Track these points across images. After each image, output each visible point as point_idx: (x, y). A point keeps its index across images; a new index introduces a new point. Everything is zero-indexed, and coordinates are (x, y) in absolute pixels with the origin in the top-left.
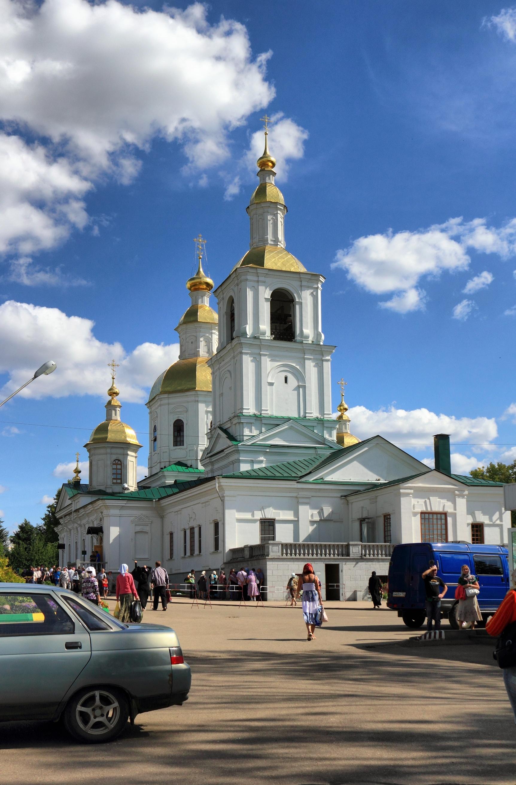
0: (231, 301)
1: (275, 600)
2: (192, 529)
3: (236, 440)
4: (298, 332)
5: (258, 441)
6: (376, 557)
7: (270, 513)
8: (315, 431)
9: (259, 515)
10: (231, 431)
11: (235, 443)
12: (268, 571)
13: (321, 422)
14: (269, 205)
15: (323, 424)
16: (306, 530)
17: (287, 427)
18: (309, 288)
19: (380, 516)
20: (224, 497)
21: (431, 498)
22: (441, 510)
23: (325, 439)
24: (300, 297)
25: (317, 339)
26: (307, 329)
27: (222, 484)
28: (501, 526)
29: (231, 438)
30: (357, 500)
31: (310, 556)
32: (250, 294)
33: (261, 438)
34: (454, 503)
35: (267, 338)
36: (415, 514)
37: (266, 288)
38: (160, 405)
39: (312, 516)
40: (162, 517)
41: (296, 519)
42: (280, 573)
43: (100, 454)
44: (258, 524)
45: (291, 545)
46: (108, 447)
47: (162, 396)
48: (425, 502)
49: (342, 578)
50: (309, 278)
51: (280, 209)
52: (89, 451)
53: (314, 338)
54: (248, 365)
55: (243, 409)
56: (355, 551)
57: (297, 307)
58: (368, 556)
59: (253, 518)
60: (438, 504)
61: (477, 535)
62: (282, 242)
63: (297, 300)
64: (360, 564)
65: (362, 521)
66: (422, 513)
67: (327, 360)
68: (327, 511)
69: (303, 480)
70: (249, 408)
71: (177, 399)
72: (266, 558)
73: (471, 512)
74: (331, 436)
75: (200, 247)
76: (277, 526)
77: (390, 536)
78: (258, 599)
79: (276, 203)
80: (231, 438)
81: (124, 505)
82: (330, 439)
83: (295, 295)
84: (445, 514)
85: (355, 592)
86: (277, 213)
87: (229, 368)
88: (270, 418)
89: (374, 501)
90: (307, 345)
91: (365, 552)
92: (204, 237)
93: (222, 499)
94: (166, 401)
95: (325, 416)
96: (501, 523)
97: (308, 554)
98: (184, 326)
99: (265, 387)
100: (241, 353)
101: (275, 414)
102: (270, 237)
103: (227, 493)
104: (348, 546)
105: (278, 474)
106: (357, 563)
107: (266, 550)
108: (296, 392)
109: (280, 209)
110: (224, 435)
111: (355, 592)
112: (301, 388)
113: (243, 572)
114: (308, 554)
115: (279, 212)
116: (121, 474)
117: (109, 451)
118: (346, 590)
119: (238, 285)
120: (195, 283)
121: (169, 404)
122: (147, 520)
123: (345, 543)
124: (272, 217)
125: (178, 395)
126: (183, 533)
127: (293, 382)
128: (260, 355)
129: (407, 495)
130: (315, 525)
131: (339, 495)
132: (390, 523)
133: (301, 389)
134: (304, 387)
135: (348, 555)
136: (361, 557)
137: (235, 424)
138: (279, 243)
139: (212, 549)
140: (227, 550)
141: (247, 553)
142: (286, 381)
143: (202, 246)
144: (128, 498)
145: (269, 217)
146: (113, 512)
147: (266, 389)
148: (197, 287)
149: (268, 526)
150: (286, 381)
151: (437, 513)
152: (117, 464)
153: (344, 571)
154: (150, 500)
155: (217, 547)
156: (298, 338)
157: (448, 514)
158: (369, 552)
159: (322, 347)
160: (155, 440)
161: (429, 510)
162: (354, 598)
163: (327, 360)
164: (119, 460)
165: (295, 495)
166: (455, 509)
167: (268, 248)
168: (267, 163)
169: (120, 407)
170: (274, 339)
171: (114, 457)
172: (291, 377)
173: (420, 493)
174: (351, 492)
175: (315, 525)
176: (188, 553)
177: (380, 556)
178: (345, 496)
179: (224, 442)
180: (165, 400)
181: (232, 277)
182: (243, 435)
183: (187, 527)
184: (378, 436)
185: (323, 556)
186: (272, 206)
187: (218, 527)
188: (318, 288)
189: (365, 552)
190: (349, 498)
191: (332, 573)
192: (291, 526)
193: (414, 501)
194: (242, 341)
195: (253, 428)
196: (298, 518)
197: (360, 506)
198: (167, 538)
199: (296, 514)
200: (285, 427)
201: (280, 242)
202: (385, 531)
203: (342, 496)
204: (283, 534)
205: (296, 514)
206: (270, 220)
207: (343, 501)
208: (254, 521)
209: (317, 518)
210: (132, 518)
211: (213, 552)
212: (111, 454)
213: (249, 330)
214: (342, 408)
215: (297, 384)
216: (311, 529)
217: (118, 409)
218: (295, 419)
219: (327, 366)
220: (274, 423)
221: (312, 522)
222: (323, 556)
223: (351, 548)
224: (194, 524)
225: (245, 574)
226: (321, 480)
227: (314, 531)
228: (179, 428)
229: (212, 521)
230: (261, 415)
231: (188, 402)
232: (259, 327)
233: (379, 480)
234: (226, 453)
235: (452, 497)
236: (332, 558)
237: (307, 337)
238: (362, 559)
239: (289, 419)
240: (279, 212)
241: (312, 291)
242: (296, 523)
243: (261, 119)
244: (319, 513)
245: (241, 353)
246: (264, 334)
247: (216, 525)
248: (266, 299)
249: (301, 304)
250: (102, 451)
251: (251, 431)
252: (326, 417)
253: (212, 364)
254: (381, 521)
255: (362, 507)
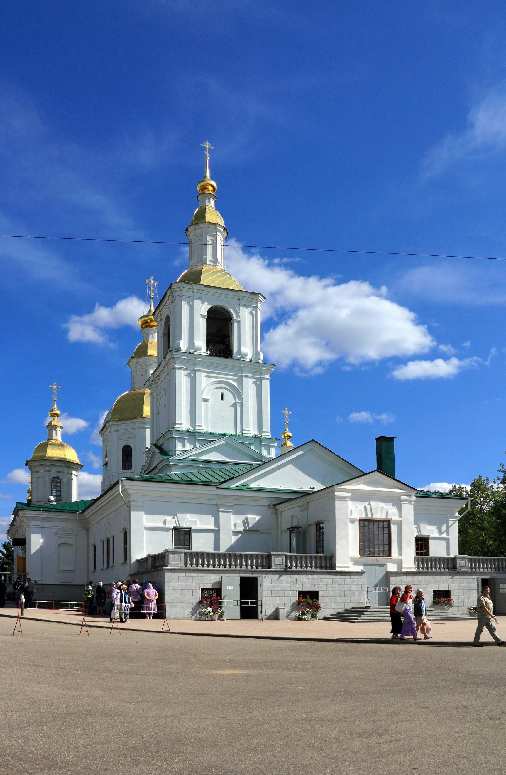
0: (168, 319)
1: (175, 619)
2: (108, 540)
3: (168, 455)
4: (235, 349)
5: (193, 454)
6: (304, 569)
7: (187, 520)
8: (253, 447)
9: (171, 522)
10: (164, 447)
11: (166, 457)
12: (166, 584)
13: (259, 440)
14: (208, 226)
15: (261, 442)
16: (228, 541)
17: (223, 442)
18: (247, 306)
19: (311, 525)
20: (129, 502)
21: (372, 503)
22: (383, 517)
23: (262, 456)
24: (238, 314)
25: (256, 357)
26: (245, 346)
27: (126, 487)
28: (447, 540)
29: (163, 452)
30: (287, 508)
31: (222, 568)
32: (185, 308)
33: (194, 453)
34: (400, 509)
35: (202, 354)
36: (353, 521)
37: (203, 303)
38: (110, 432)
39: (235, 525)
40: (88, 530)
41: (217, 529)
42: (182, 589)
43: (40, 472)
44: (171, 533)
45: (208, 554)
46: (46, 464)
47: (111, 423)
48: (365, 508)
49: (261, 593)
50: (248, 296)
51: (220, 231)
52: (30, 469)
53: (253, 356)
54: (182, 379)
55: (176, 424)
56: (278, 562)
57: (235, 325)
58: (294, 569)
59: (165, 527)
60: (381, 511)
61: (421, 549)
62: (222, 265)
63: (235, 318)
64: (285, 577)
65: (291, 530)
66: (360, 520)
67: (266, 379)
68: (254, 519)
69: (224, 485)
70: (183, 422)
71: (126, 426)
72: (163, 569)
73: (416, 522)
74: (269, 453)
75: (152, 288)
76: (193, 535)
77: (323, 546)
78: (155, 617)
79: (215, 224)
80: (163, 452)
81: (45, 516)
82: (268, 456)
83: (232, 310)
84: (389, 522)
85: (277, 610)
86: (217, 234)
87: (163, 387)
88: (205, 434)
89: (305, 508)
90: (246, 363)
91: (291, 563)
92: (155, 279)
93: (128, 504)
94: (115, 428)
95: (263, 434)
96: (448, 537)
97: (219, 565)
98: (134, 360)
99: (198, 401)
100: (175, 368)
101: (210, 430)
102: (209, 257)
103: (132, 498)
104: (269, 557)
105: (195, 479)
106: (280, 576)
107: (166, 558)
108: (233, 409)
109: (220, 231)
110: (157, 451)
111: (277, 610)
112: (239, 405)
113: (137, 585)
114: (219, 565)
115: (218, 233)
116: (61, 491)
117: (47, 468)
118: (266, 608)
119: (173, 301)
120: (146, 320)
121: (118, 431)
122: (72, 532)
123: (265, 553)
124: (211, 238)
125: (126, 422)
126: (102, 543)
127: (229, 398)
128: (195, 371)
129: (344, 498)
130: (240, 535)
131: (267, 504)
132: (323, 532)
133: (238, 407)
134: (242, 405)
135: (270, 567)
136: (286, 569)
137: (168, 439)
138: (217, 264)
139: (122, 561)
140: (133, 560)
141: (149, 562)
142: (222, 398)
143: (154, 286)
144: (49, 510)
145: (208, 238)
146: (33, 523)
147: (201, 406)
148: (148, 324)
149: (183, 536)
150: (222, 398)
151: (379, 521)
152: (56, 482)
153: (263, 586)
154: (74, 512)
155: (126, 560)
156: (235, 356)
157: (391, 522)
158: (296, 563)
159: (261, 365)
160: (106, 464)
161: (370, 517)
162: (275, 616)
163: (266, 379)
164: (58, 478)
165: (215, 502)
166: (400, 516)
167: (205, 268)
168: (207, 187)
169: (62, 427)
170: (210, 355)
171: (53, 475)
172: (228, 396)
173: (358, 496)
174: (280, 500)
175: (240, 535)
176: (106, 566)
177: (309, 569)
178: (275, 505)
179: (159, 457)
180: (114, 426)
181: (168, 294)
182: (175, 450)
183: (104, 538)
184: (313, 440)
185: (238, 568)
186: (211, 226)
187: (126, 535)
188: (257, 307)
189: (291, 563)
190: (278, 507)
191: (249, 589)
192: (212, 535)
193: (351, 505)
194: (175, 356)
195: (186, 441)
196: (219, 528)
197: (290, 515)
198: (92, 549)
199: (217, 523)
200: (222, 442)
201: (219, 263)
202: (317, 541)
203: (270, 505)
204: (201, 544)
205: (217, 523)
206: (209, 241)
207: (271, 510)
208: (168, 529)
209: (242, 529)
210: (55, 530)
211: (123, 563)
212: (50, 471)
213: (184, 345)
214: (286, 435)
215: (234, 401)
216: (234, 539)
217: (59, 429)
218: (231, 436)
219: (266, 385)
220: (208, 438)
221: (236, 533)
222: (238, 568)
223: (273, 558)
224: (109, 535)
225: (138, 586)
226: (246, 487)
227: (237, 542)
228: (127, 452)
229: (121, 530)
230: (195, 430)
231: (136, 429)
232: (194, 343)
233: (313, 488)
234: (159, 468)
235: (397, 502)
236: (250, 570)
237: (246, 355)
238: (286, 571)
239: (225, 435)
240: (218, 233)
241: (251, 309)
242: (216, 533)
243: (202, 145)
244: (243, 522)
245: (175, 368)
246: (200, 349)
247: (125, 533)
248: (202, 316)
249: (239, 322)
250: (41, 468)
251: (184, 446)
252: (264, 435)
253: (150, 385)
254: (313, 530)
255: (292, 516)
